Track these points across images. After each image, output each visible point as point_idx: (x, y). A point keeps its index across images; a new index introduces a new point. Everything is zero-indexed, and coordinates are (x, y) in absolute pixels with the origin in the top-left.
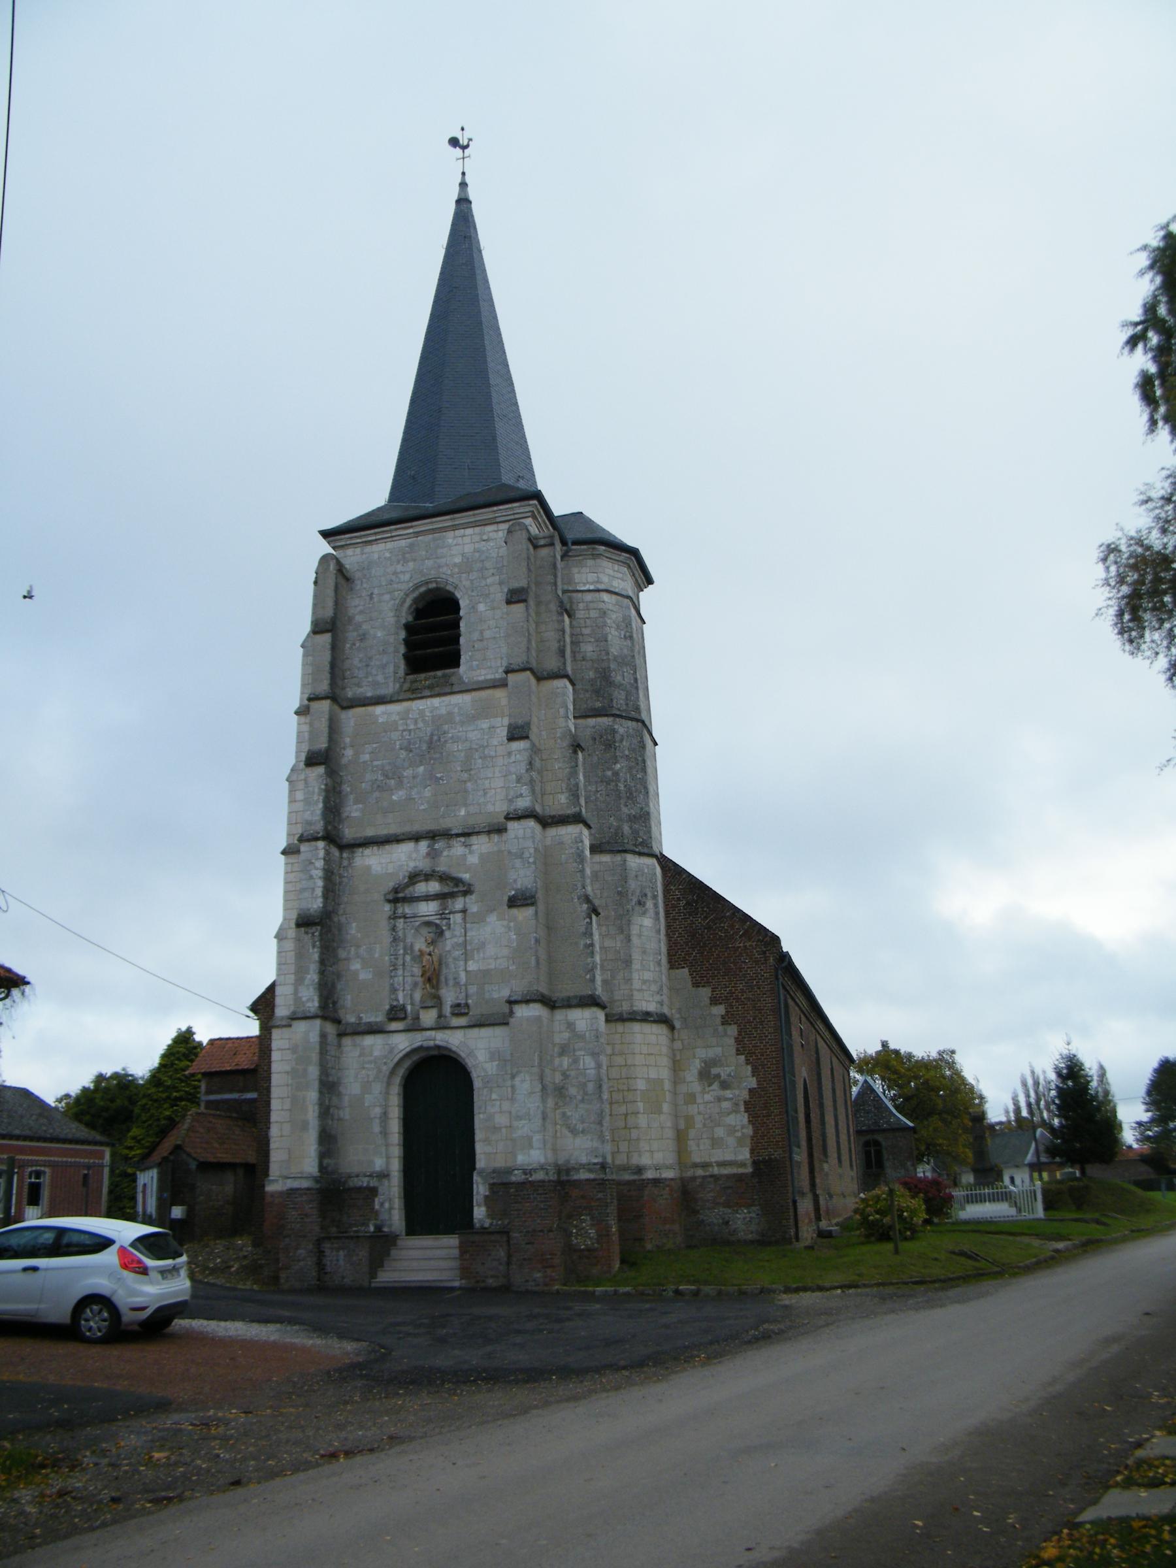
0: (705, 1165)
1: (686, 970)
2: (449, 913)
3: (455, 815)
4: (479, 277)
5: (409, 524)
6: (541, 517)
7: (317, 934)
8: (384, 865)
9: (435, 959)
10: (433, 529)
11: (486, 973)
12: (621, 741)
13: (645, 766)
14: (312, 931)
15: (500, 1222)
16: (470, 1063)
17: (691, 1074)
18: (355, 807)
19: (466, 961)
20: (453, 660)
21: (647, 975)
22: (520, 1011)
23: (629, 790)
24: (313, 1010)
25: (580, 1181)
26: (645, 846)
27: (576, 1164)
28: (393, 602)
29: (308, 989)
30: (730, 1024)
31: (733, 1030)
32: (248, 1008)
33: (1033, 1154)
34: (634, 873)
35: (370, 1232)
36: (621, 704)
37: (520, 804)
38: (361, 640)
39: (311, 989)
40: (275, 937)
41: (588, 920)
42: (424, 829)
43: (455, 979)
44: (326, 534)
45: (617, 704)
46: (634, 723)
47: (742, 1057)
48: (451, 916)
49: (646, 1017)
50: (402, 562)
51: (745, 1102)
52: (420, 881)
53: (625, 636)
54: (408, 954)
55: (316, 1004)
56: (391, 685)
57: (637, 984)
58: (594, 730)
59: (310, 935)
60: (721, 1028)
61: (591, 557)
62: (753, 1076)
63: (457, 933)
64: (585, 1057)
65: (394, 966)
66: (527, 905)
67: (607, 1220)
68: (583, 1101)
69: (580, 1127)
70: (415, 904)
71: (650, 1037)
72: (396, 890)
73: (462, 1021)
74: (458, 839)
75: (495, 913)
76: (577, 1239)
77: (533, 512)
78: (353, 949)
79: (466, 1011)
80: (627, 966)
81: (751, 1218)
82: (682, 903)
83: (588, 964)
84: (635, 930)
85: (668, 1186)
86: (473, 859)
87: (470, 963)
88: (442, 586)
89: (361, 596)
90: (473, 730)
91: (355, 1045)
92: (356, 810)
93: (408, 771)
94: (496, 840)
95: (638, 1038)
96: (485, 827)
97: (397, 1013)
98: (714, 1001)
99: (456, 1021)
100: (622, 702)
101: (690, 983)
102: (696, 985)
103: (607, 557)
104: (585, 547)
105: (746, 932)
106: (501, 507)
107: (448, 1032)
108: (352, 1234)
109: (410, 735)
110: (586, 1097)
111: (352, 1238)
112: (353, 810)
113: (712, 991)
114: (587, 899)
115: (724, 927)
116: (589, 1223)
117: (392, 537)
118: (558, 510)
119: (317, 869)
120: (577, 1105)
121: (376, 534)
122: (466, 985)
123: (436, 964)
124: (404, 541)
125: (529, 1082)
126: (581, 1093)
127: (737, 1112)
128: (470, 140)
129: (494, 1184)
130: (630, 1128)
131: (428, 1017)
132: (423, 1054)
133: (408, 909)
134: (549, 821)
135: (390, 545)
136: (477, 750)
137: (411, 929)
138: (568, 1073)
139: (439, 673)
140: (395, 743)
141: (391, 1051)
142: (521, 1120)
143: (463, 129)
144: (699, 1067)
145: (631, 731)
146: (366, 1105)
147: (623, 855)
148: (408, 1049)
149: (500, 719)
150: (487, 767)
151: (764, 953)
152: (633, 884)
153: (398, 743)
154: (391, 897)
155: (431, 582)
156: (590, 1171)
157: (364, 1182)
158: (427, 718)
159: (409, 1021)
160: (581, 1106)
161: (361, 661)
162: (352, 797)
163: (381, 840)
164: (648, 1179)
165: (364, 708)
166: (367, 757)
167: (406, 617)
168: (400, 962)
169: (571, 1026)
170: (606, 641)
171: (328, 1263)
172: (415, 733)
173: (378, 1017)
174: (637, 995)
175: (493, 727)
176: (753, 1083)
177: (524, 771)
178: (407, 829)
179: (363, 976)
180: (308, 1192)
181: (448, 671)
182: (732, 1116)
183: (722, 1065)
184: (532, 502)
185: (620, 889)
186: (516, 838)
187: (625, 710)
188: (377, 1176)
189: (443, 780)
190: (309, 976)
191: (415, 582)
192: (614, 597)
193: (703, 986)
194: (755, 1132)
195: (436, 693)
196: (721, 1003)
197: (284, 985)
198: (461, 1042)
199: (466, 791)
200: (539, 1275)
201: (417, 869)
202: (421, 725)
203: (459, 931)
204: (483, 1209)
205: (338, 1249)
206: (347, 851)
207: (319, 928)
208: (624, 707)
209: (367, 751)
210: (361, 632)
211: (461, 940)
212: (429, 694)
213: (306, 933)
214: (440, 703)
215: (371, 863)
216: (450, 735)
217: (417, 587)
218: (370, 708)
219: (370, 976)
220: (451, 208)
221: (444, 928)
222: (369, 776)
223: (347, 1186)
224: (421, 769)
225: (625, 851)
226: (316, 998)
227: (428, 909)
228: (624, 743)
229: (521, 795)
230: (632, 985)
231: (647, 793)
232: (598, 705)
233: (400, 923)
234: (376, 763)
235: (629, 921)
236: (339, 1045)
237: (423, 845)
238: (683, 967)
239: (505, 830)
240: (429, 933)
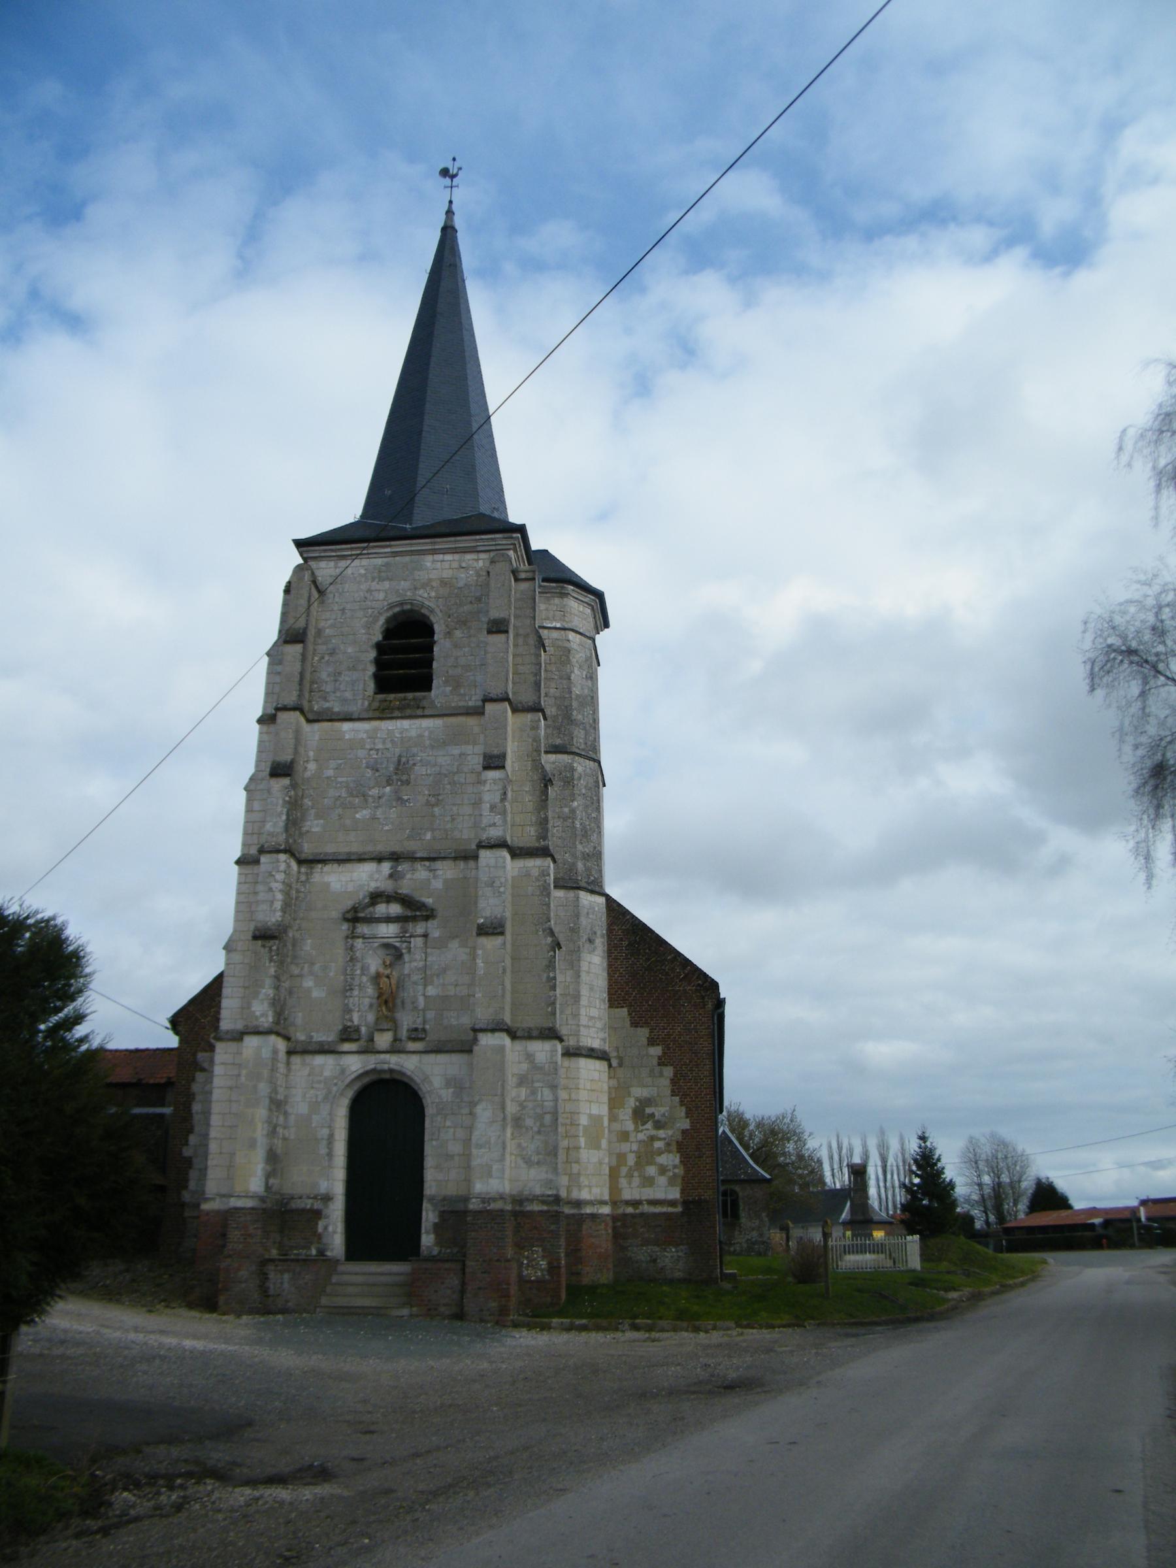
0: (636, 1203)
1: (625, 1010)
2: (410, 937)
3: (420, 839)
4: (462, 306)
5: (388, 543)
6: (521, 551)
7: (274, 948)
8: (343, 883)
9: (393, 981)
10: (411, 551)
11: (445, 999)
12: (580, 778)
13: (599, 806)
14: (270, 944)
15: (448, 1251)
16: (424, 1089)
17: (626, 1114)
18: (316, 822)
19: (425, 986)
20: (425, 684)
21: (594, 1012)
22: (485, 1039)
23: (584, 829)
24: (266, 1025)
25: (531, 1213)
26: (596, 888)
27: (530, 1195)
28: (366, 619)
29: (263, 1004)
30: (666, 1065)
31: (669, 1071)
32: (167, 1019)
33: (847, 1213)
34: (586, 911)
35: (311, 1256)
36: (580, 743)
37: (492, 832)
38: (331, 654)
39: (266, 1004)
40: (224, 948)
41: (552, 953)
42: (388, 850)
43: (413, 1003)
44: (300, 544)
45: (577, 742)
46: (591, 763)
47: (677, 1099)
48: (412, 939)
49: (591, 1054)
50: (377, 580)
51: (677, 1142)
52: (381, 902)
53: (586, 676)
54: (364, 975)
55: (271, 1019)
56: (360, 702)
57: (584, 1020)
58: (554, 766)
59: (267, 949)
60: (657, 1069)
61: (558, 595)
62: (687, 1117)
63: (418, 957)
64: (544, 1089)
65: (349, 985)
66: (493, 934)
67: (559, 1252)
68: (539, 1132)
69: (535, 1159)
70: (374, 924)
71: (591, 1072)
72: (355, 909)
73: (418, 1046)
74: (423, 863)
75: (458, 940)
76: (527, 1270)
77: (515, 544)
78: (306, 965)
79: (424, 1036)
80: (575, 1001)
81: (679, 1257)
82: (625, 943)
83: (550, 997)
84: (584, 966)
85: (603, 1221)
86: (438, 884)
87: (429, 988)
88: (417, 609)
89: (332, 610)
90: (444, 756)
91: (304, 1064)
92: (317, 826)
93: (373, 790)
94: (462, 868)
95: (583, 1074)
96: (451, 853)
97: (348, 1034)
98: (652, 1042)
99: (412, 1046)
100: (581, 741)
101: (629, 1022)
102: (635, 1024)
103: (574, 597)
104: (554, 585)
105: (686, 976)
106: (483, 537)
107: (403, 1056)
108: (292, 1257)
109: (377, 754)
110: (542, 1129)
111: (292, 1260)
112: (314, 825)
113: (650, 1032)
114: (552, 933)
115: (664, 970)
116: (541, 1253)
117: (368, 554)
118: (535, 545)
119: (276, 881)
120: (533, 1137)
121: (352, 549)
122: (424, 1010)
123: (394, 987)
124: (381, 559)
125: (491, 1111)
126: (538, 1124)
127: (670, 1152)
128: (460, 169)
129: (444, 1212)
130: (571, 1163)
131: (383, 1040)
132: (373, 1077)
133: (363, 929)
134: (518, 852)
135: (365, 562)
136: (446, 776)
137: (369, 950)
138: (525, 1104)
139: (410, 695)
140: (361, 761)
141: (343, 1071)
142: (481, 1148)
143: (454, 159)
144: (634, 1106)
145: (588, 770)
146: (313, 1125)
147: (576, 891)
148: (360, 1071)
149: (471, 747)
150: (456, 793)
151: (703, 998)
152: (583, 921)
153: (364, 761)
154: (349, 916)
155: (406, 603)
156: (544, 1202)
157: (308, 1204)
158: (396, 739)
159: (362, 1043)
160: (537, 1137)
161: (329, 675)
162: (313, 812)
163: (341, 857)
164: (587, 1214)
165: (330, 724)
166: (330, 773)
167: (378, 637)
168: (357, 982)
169: (530, 1057)
170: (570, 679)
171: (272, 1286)
172: (383, 753)
173: (325, 1036)
174: (583, 1031)
175: (464, 754)
176: (685, 1124)
177: (498, 801)
178: (369, 848)
179: (316, 994)
180: (254, 1212)
181: (418, 694)
182: (664, 1156)
183: (656, 1106)
184: (515, 535)
185: (572, 925)
186: (488, 866)
187: (583, 750)
188: (321, 1199)
189: (410, 803)
190: (264, 991)
191: (390, 601)
192: (578, 636)
193: (641, 1027)
194: (687, 1171)
195: (407, 714)
196: (658, 1045)
197: (232, 997)
198: (416, 1067)
199: (433, 816)
200: (494, 1304)
201: (379, 890)
202: (389, 745)
203: (419, 955)
204: (432, 1237)
205: (282, 1272)
206: (305, 866)
207: (277, 942)
208: (583, 746)
209: (331, 766)
210: (330, 646)
211: (421, 964)
212: (400, 715)
213: (263, 946)
214: (410, 725)
215: (330, 880)
216: (419, 758)
217: (391, 607)
218: (337, 724)
219: (323, 995)
220: (437, 236)
221: (404, 951)
222: (332, 793)
223: (288, 1208)
224: (388, 789)
225: (579, 888)
226: (270, 1013)
227: (388, 931)
228: (582, 782)
229: (494, 824)
230: (579, 1020)
231: (600, 832)
232: (558, 741)
233: (359, 943)
234: (340, 779)
235: (579, 957)
236: (288, 1063)
237: (386, 867)
238: (622, 1007)
239: (476, 857)
240: (387, 955)
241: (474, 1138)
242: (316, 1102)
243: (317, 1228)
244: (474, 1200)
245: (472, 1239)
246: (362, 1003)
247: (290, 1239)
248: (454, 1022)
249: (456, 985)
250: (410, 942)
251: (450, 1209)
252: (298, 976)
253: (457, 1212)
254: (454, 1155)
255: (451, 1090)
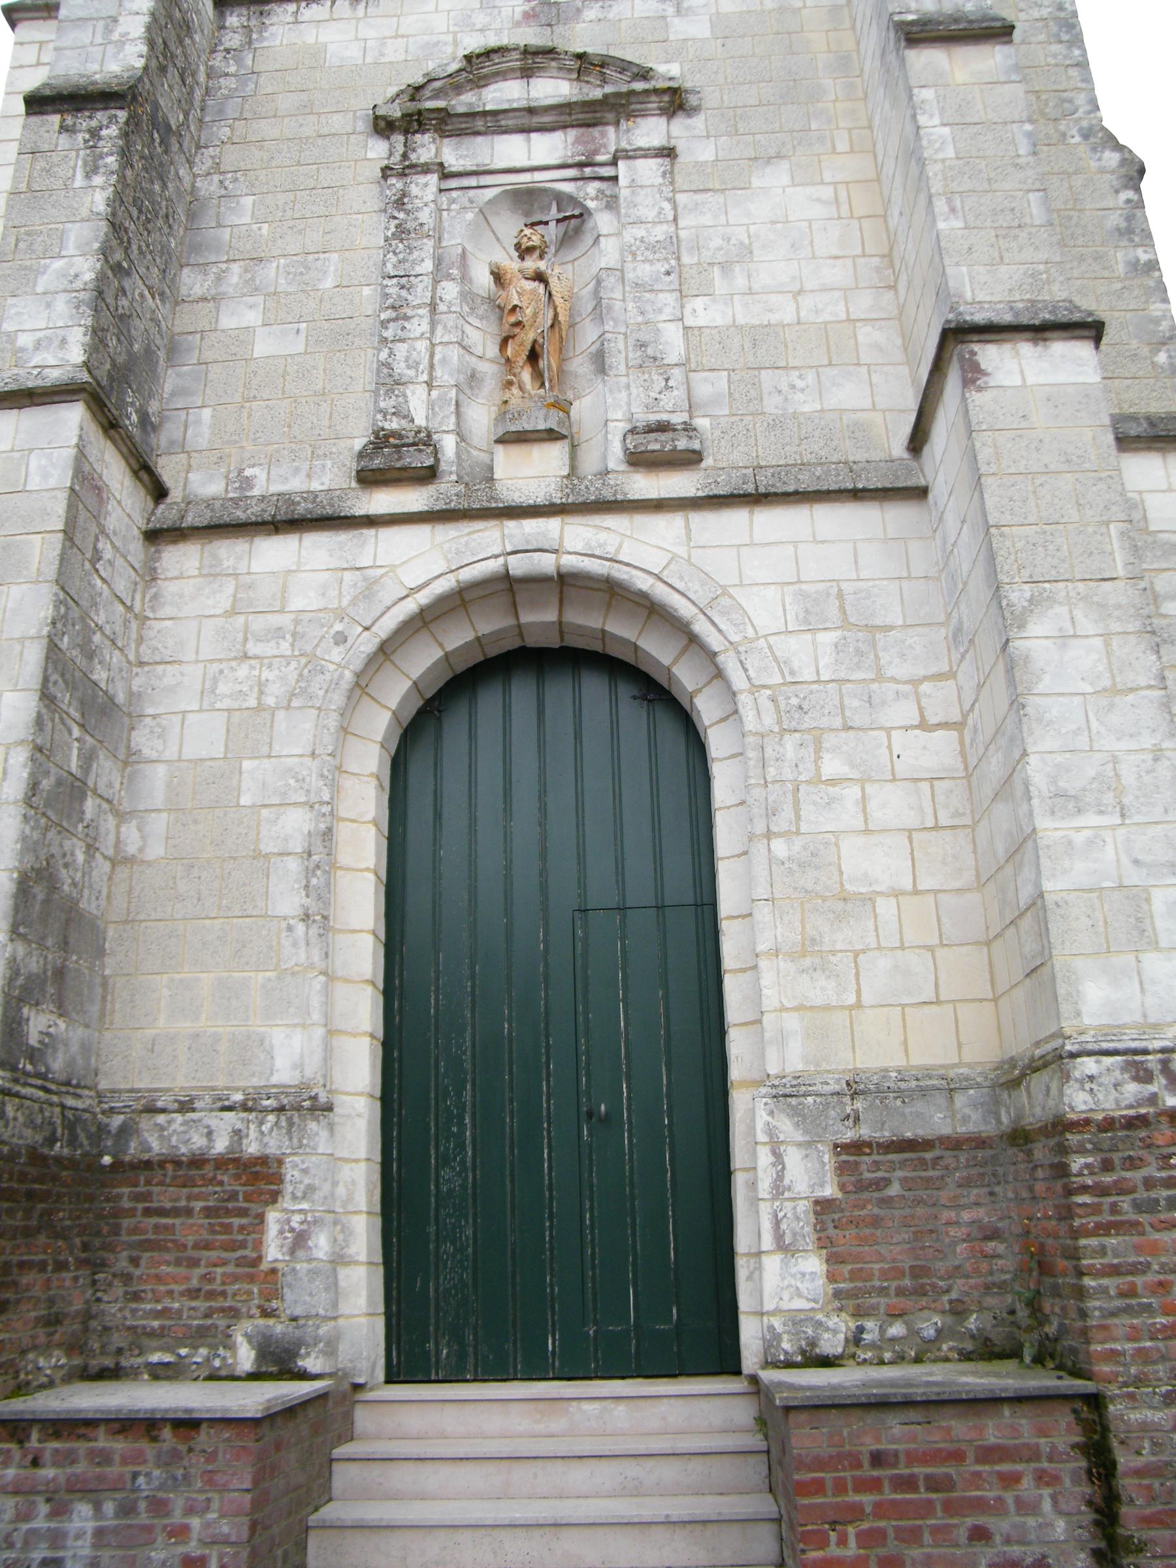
39: (61, 305)
75: (785, 165)
78: (236, 268)
91: (212, 575)
107: (616, 522)
129: (857, 1147)
141: (369, 591)
146: (245, 800)
233: (425, 188)
236: (150, 575)
241: (1037, 771)
242: (260, 708)
243: (258, 1244)
244: (1089, 1065)
245: (1114, 1271)
246: (444, 360)
247: (136, 1297)
248: (807, 405)
249: (800, 292)
250: (615, 179)
251: (886, 1135)
252: (204, 299)
253: (925, 1145)
254: (869, 900)
255: (827, 638)
